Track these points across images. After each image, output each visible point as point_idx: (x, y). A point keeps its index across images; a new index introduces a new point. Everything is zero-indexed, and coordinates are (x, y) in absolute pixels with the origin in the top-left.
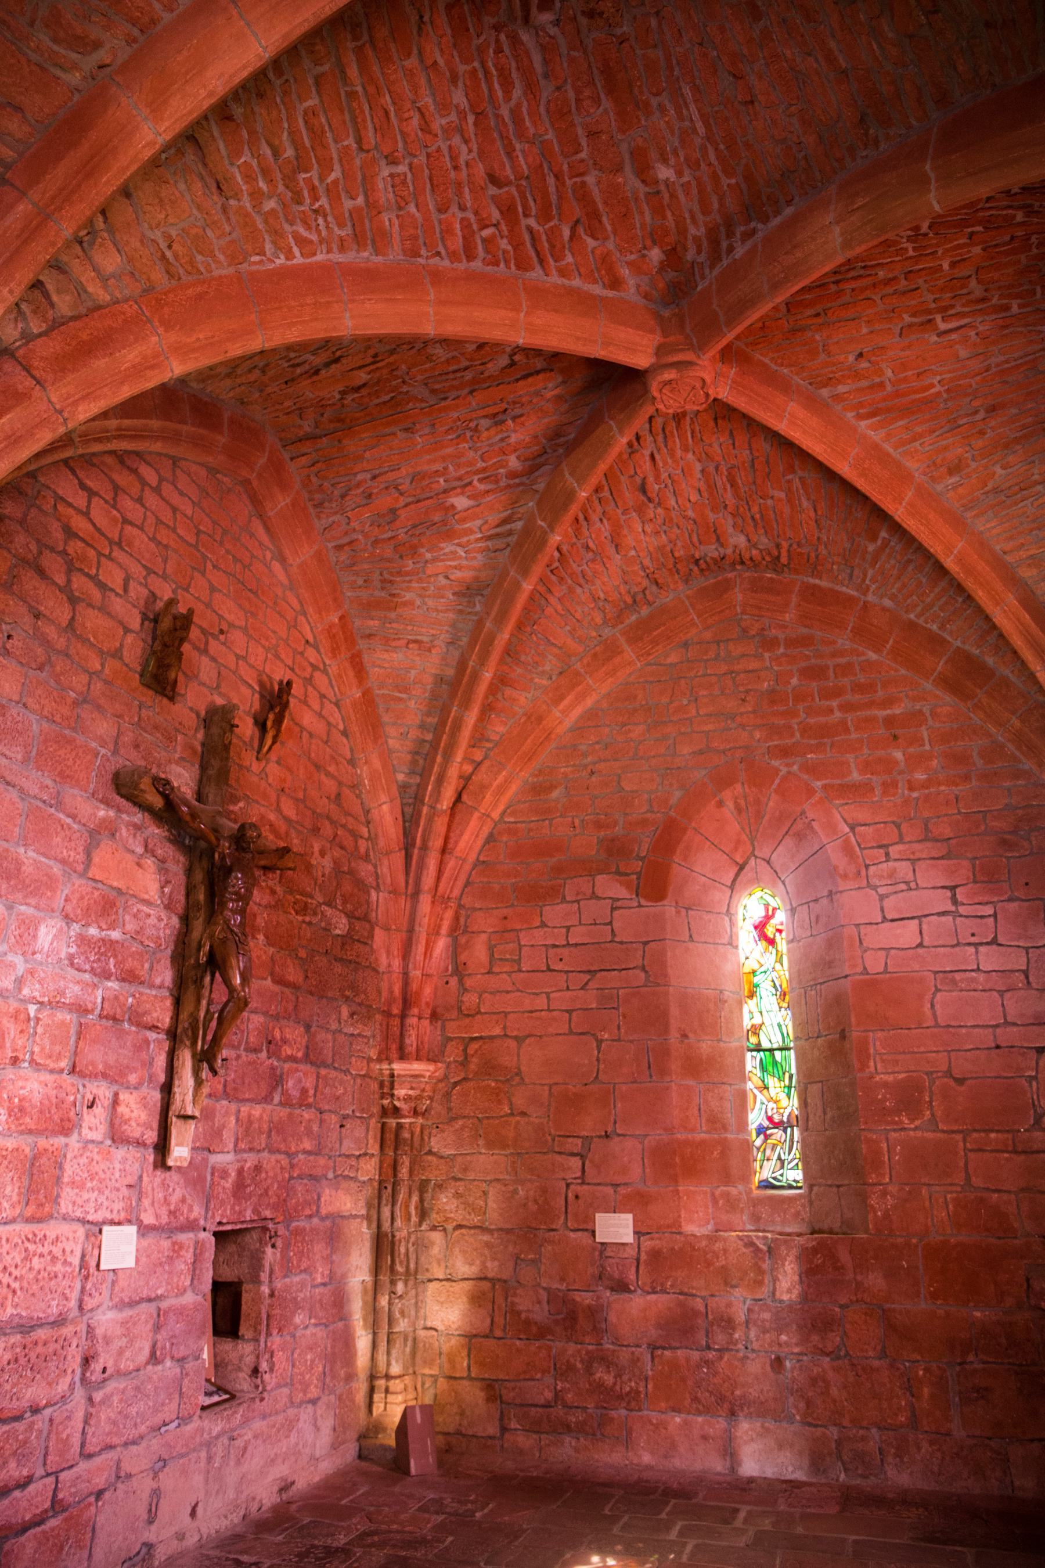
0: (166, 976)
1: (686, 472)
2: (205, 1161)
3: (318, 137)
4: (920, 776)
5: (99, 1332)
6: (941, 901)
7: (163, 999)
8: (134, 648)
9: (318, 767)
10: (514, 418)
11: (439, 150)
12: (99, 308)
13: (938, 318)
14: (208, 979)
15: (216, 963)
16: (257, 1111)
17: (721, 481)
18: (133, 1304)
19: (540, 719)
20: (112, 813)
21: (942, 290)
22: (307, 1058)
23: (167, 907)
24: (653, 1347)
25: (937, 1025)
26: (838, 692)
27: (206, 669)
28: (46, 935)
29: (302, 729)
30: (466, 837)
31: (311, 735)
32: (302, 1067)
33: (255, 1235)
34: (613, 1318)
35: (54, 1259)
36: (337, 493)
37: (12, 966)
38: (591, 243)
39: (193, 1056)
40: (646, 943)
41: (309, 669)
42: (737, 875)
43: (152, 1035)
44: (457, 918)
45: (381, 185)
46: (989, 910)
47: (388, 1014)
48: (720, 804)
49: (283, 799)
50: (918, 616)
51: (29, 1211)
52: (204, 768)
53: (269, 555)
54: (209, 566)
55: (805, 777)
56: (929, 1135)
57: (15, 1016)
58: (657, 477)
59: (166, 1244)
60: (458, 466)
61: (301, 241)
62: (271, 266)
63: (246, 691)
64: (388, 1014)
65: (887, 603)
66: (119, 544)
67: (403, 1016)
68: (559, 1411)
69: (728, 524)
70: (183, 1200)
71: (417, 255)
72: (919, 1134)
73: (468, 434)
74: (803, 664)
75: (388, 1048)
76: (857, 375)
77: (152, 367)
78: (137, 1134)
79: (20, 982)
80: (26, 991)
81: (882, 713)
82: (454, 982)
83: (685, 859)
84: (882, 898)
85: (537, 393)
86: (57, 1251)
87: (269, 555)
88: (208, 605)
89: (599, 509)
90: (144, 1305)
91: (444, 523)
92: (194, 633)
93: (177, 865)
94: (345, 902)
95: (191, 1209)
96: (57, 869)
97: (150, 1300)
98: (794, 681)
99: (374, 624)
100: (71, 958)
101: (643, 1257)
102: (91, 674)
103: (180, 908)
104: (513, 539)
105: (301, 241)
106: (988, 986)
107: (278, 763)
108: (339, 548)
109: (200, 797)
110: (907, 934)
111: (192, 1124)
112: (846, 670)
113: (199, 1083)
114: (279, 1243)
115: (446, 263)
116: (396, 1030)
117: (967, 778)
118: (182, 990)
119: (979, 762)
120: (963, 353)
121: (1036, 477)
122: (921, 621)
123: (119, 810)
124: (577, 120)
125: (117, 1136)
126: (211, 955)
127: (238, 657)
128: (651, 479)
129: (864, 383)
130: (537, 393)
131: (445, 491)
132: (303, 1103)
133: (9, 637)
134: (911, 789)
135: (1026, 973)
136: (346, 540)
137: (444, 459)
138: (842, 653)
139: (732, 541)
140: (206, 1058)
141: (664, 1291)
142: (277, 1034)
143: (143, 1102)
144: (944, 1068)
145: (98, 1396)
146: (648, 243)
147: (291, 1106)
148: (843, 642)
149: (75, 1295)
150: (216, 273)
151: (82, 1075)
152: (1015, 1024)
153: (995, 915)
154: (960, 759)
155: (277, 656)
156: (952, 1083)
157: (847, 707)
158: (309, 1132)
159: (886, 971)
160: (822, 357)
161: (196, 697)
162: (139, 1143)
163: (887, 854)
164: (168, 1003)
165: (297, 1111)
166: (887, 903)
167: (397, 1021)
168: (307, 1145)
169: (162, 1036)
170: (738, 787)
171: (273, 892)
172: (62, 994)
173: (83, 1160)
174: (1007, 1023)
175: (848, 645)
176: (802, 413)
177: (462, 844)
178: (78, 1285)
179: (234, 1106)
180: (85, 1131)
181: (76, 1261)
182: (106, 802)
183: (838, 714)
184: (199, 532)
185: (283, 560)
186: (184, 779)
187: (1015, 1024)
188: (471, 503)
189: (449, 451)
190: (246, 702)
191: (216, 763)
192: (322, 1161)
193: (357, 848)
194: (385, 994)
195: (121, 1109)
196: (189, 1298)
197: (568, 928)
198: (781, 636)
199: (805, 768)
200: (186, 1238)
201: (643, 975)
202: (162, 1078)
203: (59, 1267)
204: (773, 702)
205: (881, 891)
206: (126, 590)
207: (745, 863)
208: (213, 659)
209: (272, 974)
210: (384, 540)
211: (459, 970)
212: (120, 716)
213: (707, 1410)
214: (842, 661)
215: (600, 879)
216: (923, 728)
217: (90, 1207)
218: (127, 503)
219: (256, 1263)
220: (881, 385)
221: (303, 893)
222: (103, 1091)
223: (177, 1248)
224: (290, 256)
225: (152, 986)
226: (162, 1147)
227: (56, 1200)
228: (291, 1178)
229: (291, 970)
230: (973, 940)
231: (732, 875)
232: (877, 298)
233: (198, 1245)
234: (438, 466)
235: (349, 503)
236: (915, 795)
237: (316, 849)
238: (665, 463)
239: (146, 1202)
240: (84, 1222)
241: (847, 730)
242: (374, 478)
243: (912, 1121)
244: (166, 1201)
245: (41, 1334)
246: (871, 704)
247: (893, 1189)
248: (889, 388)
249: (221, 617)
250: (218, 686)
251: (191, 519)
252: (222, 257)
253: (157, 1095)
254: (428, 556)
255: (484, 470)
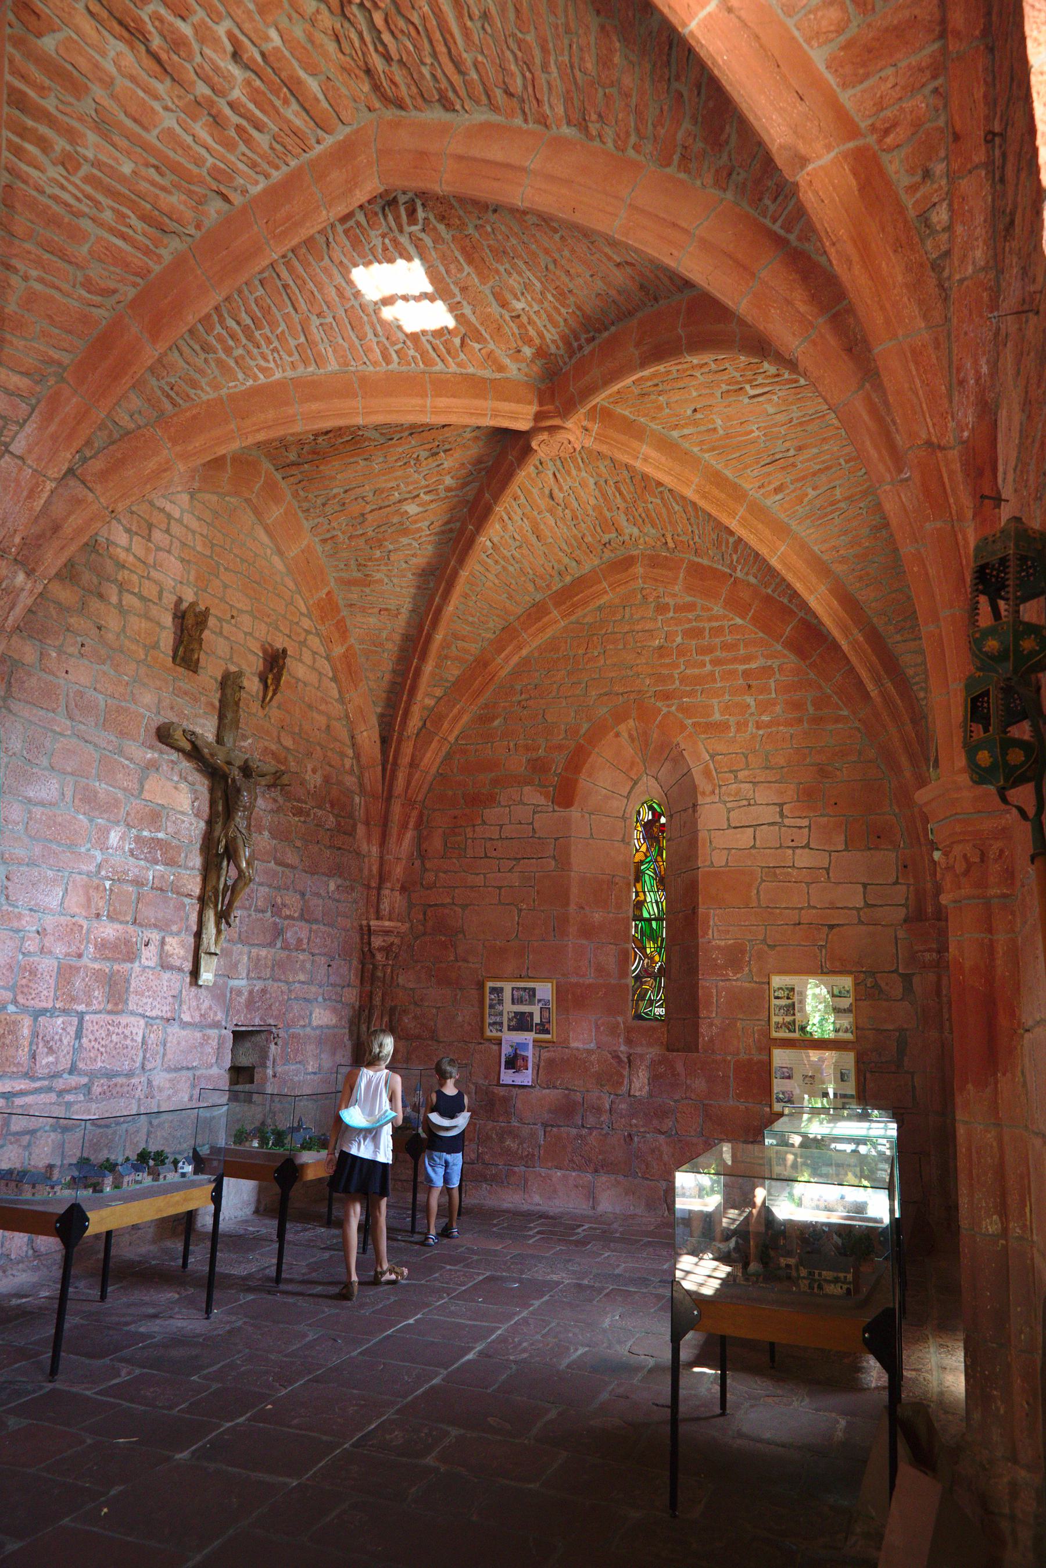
0: (196, 861)
1: (583, 484)
2: (226, 984)
3: (266, 311)
4: (765, 718)
5: (155, 1083)
6: (770, 814)
7: (194, 877)
8: (167, 639)
9: (310, 706)
10: (445, 451)
11: (353, 306)
12: (128, 433)
13: (747, 387)
14: (225, 863)
15: (231, 854)
16: (263, 952)
17: (610, 491)
18: (177, 1070)
19: (486, 665)
20: (156, 755)
21: (743, 370)
22: (302, 917)
23: (196, 815)
24: (545, 1125)
25: (760, 907)
26: (709, 650)
27: (221, 647)
28: (114, 837)
29: (298, 680)
30: (428, 755)
31: (305, 684)
32: (297, 923)
33: (263, 1036)
34: (519, 1105)
35: (126, 1037)
36: (319, 502)
37: (94, 857)
38: (477, 346)
39: (216, 914)
40: (556, 839)
41: (304, 634)
42: (632, 788)
43: (187, 901)
44: (421, 815)
45: (315, 331)
46: (805, 822)
47: (368, 887)
48: (617, 735)
49: (282, 734)
50: (774, 591)
51: (110, 1007)
52: (221, 717)
53: (269, 552)
54: (222, 569)
55: (680, 716)
56: (747, 985)
57: (97, 888)
58: (561, 489)
59: (198, 1035)
60: (407, 484)
61: (263, 370)
62: (244, 388)
63: (252, 658)
64: (368, 887)
65: (752, 580)
66: (154, 566)
67: (379, 888)
68: (478, 1167)
69: (622, 519)
70: (210, 1008)
71: (348, 365)
72: (739, 984)
73: (412, 462)
74: (687, 626)
75: (368, 912)
76: (695, 423)
77: (165, 470)
78: (178, 963)
79: (99, 867)
80: (103, 873)
81: (741, 667)
82: (418, 863)
83: (590, 776)
84: (729, 811)
85: (459, 435)
86: (127, 1032)
87: (269, 552)
88: (222, 599)
89: (519, 512)
90: (184, 1073)
91: (401, 523)
92: (212, 622)
93: (202, 785)
94: (332, 806)
95: (216, 1014)
96: (120, 795)
97: (188, 1069)
98: (679, 640)
99: (354, 596)
100: (131, 851)
101: (542, 1064)
102: (138, 662)
103: (206, 816)
104: (454, 535)
105: (263, 370)
106: (799, 879)
107: (279, 708)
108: (324, 541)
109: (219, 740)
110: (745, 838)
111: (215, 959)
112: (717, 632)
113: (219, 932)
114: (280, 1042)
115: (371, 368)
116: (374, 899)
117: (800, 721)
118: (210, 868)
119: (811, 710)
120: (771, 410)
121: (839, 497)
122: (775, 595)
123: (161, 752)
124: (449, 280)
125: (165, 965)
126: (226, 847)
127: (246, 633)
128: (556, 491)
129: (703, 428)
130: (459, 435)
131: (400, 501)
132: (298, 948)
133: (83, 645)
134: (758, 728)
135: (827, 870)
136: (328, 535)
137: (396, 479)
138: (716, 618)
139: (627, 531)
140: (223, 916)
141: (555, 1087)
142: (279, 901)
143: (182, 944)
144: (761, 937)
145: (155, 1122)
146: (520, 343)
147: (290, 950)
148: (718, 609)
149: (139, 1060)
150: (205, 398)
151: (141, 925)
152: (815, 907)
153: (810, 827)
154: (797, 706)
155: (277, 628)
156: (766, 948)
157: (716, 662)
158: (303, 969)
159: (727, 865)
160: (667, 411)
161: (211, 670)
162: (180, 970)
163: (736, 777)
164: (199, 879)
165: (294, 954)
166: (732, 814)
167: (375, 892)
168: (302, 977)
169: (195, 901)
170: (631, 723)
171: (275, 801)
172: (126, 873)
173: (143, 978)
174: (810, 907)
175: (722, 611)
176: (654, 454)
177: (426, 760)
178: (141, 1054)
179: (246, 949)
180: (143, 960)
181: (139, 1039)
182: (151, 747)
183: (709, 667)
184: (213, 545)
185: (280, 553)
186: (206, 729)
187: (815, 907)
188: (421, 509)
189: (399, 473)
190: (251, 666)
191: (230, 715)
192: (314, 989)
193: (343, 766)
194: (366, 872)
195: (167, 947)
196: (215, 1071)
197: (501, 826)
198: (672, 602)
199: (681, 708)
200: (213, 1032)
201: (553, 863)
202: (195, 928)
203: (128, 1042)
204: (661, 656)
205: (729, 805)
206: (160, 599)
207: (639, 779)
208: (227, 638)
209: (275, 858)
210: (358, 536)
211: (423, 855)
212: (160, 689)
213: (580, 1169)
214: (715, 624)
215: (527, 789)
216: (772, 681)
217: (148, 1007)
218: (157, 535)
219: (264, 1055)
220: (715, 429)
221: (299, 800)
222: (155, 936)
223: (206, 1038)
224: (255, 378)
225: (186, 868)
226: (195, 973)
227: (126, 1002)
228: (289, 999)
229: (289, 855)
230: (791, 844)
231: (628, 789)
232: (698, 374)
233: (221, 1039)
234: (393, 484)
235: (329, 509)
236: (761, 732)
237: (309, 767)
238: (565, 480)
239: (185, 1007)
240: (144, 1016)
241: (714, 681)
242: (346, 491)
243: (735, 974)
244: (198, 1008)
245: (120, 1080)
246: (735, 660)
247: (717, 1022)
248: (721, 432)
249: (232, 606)
250: (231, 658)
251: (206, 537)
252: (208, 389)
253: (191, 940)
254: (391, 547)
255: (427, 486)
